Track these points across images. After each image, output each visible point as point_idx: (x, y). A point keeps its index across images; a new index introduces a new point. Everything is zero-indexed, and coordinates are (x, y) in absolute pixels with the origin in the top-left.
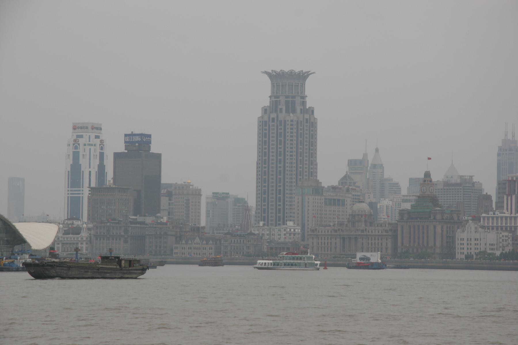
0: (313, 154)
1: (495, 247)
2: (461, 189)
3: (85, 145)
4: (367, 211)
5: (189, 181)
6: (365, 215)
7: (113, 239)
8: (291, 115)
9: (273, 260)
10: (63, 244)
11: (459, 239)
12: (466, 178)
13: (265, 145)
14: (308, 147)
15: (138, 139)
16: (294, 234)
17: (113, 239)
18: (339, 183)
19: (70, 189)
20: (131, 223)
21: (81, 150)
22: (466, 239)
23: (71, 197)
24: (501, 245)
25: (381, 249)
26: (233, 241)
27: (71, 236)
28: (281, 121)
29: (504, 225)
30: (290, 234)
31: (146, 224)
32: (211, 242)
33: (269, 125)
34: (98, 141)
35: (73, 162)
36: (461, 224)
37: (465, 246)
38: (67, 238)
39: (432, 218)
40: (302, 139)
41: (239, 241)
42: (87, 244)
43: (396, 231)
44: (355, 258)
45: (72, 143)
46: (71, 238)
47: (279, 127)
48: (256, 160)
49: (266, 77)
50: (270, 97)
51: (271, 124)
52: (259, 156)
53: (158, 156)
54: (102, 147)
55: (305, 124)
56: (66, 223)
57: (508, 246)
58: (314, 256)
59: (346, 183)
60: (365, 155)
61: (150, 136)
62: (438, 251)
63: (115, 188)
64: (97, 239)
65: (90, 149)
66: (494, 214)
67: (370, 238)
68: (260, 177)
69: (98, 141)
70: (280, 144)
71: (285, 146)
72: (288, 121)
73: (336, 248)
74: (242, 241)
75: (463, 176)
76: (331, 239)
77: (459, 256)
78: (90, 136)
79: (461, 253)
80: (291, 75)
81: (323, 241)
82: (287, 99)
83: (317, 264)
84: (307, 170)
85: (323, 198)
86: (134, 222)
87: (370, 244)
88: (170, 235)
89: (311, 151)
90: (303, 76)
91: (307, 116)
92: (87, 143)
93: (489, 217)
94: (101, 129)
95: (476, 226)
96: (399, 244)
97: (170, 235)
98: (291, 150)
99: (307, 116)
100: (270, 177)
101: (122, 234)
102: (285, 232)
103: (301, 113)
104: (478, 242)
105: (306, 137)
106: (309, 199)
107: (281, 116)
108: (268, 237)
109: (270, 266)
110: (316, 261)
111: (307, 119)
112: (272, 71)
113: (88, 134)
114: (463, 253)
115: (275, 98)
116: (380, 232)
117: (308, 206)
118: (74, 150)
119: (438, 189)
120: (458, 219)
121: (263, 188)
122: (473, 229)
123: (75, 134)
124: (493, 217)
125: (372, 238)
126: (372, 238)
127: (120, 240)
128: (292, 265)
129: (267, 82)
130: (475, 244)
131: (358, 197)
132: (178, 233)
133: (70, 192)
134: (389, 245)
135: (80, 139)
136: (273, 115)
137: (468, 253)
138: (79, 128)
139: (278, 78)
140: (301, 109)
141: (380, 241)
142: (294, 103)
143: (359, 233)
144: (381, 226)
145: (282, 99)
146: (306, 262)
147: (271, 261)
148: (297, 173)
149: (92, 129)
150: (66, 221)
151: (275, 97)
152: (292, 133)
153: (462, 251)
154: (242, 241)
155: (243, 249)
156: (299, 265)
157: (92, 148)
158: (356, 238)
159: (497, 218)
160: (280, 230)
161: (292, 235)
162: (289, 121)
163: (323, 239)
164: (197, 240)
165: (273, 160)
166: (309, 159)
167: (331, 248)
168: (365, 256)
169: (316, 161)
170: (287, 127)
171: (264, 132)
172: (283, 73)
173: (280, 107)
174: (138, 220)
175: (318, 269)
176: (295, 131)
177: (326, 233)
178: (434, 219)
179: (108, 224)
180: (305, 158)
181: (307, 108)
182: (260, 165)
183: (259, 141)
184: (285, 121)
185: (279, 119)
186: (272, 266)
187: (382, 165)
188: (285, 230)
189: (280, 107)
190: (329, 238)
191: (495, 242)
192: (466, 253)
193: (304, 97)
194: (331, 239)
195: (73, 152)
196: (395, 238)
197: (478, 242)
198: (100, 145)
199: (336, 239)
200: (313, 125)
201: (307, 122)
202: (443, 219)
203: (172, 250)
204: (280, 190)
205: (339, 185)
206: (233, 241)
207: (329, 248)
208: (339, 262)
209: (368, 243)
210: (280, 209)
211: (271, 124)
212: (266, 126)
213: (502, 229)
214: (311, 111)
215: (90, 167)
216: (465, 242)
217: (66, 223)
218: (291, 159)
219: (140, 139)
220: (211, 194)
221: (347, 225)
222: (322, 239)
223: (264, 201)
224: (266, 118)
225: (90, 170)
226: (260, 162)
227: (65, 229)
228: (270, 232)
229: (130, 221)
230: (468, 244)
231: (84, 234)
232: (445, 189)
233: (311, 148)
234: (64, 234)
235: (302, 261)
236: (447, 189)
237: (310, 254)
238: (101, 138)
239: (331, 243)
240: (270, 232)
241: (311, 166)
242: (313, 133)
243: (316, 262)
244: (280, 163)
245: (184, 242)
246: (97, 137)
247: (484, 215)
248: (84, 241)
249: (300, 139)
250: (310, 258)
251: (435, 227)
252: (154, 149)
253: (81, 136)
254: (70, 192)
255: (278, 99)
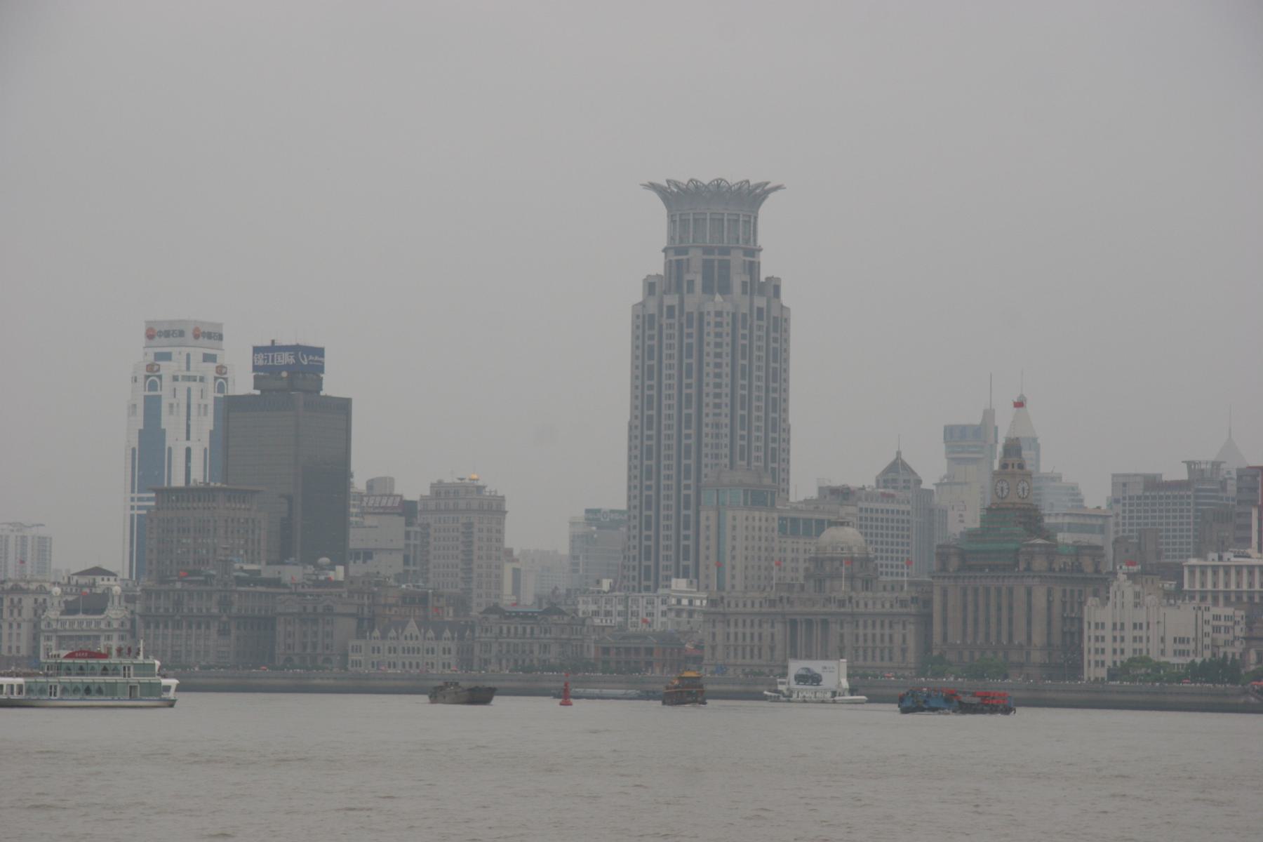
0: (777, 403)
1: (1192, 646)
2: (1189, 497)
3: (175, 379)
4: (855, 549)
5: (475, 476)
6: (851, 560)
7: (190, 627)
8: (718, 298)
9: (24, 675)
10: (61, 638)
11: (1093, 626)
12: (1203, 466)
13: (651, 378)
14: (763, 384)
15: (287, 359)
16: (691, 614)
17: (190, 627)
18: (878, 481)
19: (136, 495)
20: (240, 581)
21: (165, 392)
22: (1109, 625)
23: (139, 515)
24: (1207, 641)
25: (891, 652)
26: (505, 631)
27: (81, 616)
28: (690, 315)
29: (1233, 587)
30: (679, 613)
31: (285, 586)
32: (447, 634)
33: (661, 326)
34: (210, 370)
35: (145, 425)
36: (1100, 583)
37: (1108, 645)
38: (72, 623)
39: (1021, 568)
40: (746, 362)
41: (520, 630)
42: (122, 638)
43: (928, 603)
44: (784, 675)
45: (142, 372)
46: (81, 623)
47: (685, 330)
48: (628, 417)
49: (654, 197)
50: (665, 250)
51: (665, 321)
52: (634, 407)
53: (343, 407)
54: (221, 384)
55: (756, 323)
56: (73, 582)
57: (1233, 642)
58: (157, 663)
59: (894, 481)
60: (989, 414)
61: (320, 352)
62: (1037, 656)
63: (219, 489)
64: (148, 626)
65: (189, 390)
66: (1220, 558)
67: (861, 623)
68: (637, 462)
69: (210, 370)
70: (689, 376)
71: (700, 380)
72: (709, 313)
73: (772, 649)
74: (528, 631)
75: (1194, 463)
76: (760, 625)
77: (1092, 672)
78: (188, 355)
79: (1097, 662)
80: (718, 192)
81: (740, 630)
82: (705, 257)
83: (167, 688)
84: (761, 444)
85: (776, 515)
86: (254, 579)
87: (861, 638)
88: (344, 615)
89: (772, 395)
90: (751, 197)
91: (760, 302)
92: (180, 374)
93: (1206, 566)
94: (220, 337)
95: (1138, 588)
96: (937, 639)
97: (344, 615)
98: (717, 391)
99: (760, 302)
100: (664, 462)
101: (215, 611)
102: (664, 608)
103: (744, 292)
104: (1143, 633)
105: (759, 358)
106: (734, 519)
107: (691, 302)
108: (620, 619)
109: (15, 696)
110: (165, 677)
111: (760, 310)
112: (668, 181)
113: (185, 350)
114: (1103, 663)
115: (676, 251)
116: (887, 605)
117: (734, 538)
118: (147, 393)
119: (1131, 498)
120: (1097, 571)
121: (645, 493)
122: (1129, 597)
123: (151, 351)
124: (1218, 566)
125: (865, 622)
126: (865, 622)
127: (208, 627)
128: (88, 691)
129: (657, 212)
130: (1135, 639)
131: (905, 517)
132: (366, 610)
133: (136, 504)
134: (911, 643)
135: (163, 364)
136: (672, 300)
137: (1115, 663)
138: (161, 334)
139: (678, 198)
140: (744, 284)
141: (887, 631)
142: (725, 266)
143: (833, 608)
144: (893, 589)
145: (696, 257)
146: (134, 680)
147: (20, 680)
148: (732, 453)
149: (196, 336)
150: (75, 578)
151: (679, 251)
152: (718, 345)
153: (1100, 658)
154: (528, 631)
155: (532, 652)
156: (112, 690)
157: (195, 386)
158: (825, 623)
159: (1227, 569)
160: (651, 602)
161: (685, 615)
162: (712, 314)
163: (740, 624)
164: (412, 628)
165: (669, 417)
166: (766, 414)
167: (760, 650)
168: (808, 669)
169: (785, 420)
170: (706, 329)
171: (648, 343)
172: (697, 187)
173: (687, 277)
174: (264, 575)
175: (171, 704)
176: (729, 339)
177: (749, 609)
178: (1028, 569)
179: (178, 585)
180: (755, 414)
181: (762, 279)
182: (638, 432)
183: (635, 367)
184: (701, 315)
185: (687, 309)
186: (23, 696)
187: (1035, 440)
188: (664, 602)
189: (687, 277)
190: (756, 622)
191: (1192, 635)
192: (1109, 663)
193: (753, 252)
194: (760, 625)
195: (146, 397)
196: (925, 620)
197: (1143, 633)
198: (216, 379)
199: (773, 626)
200: (778, 324)
201: (760, 317)
202: (1051, 569)
203: (345, 655)
204: (687, 497)
205: (878, 487)
206: (505, 631)
207: (756, 651)
208: (589, 691)
209: (728, 634)
210: (687, 548)
211: (665, 321)
212: (651, 328)
213: (1227, 598)
214: (774, 288)
215: (188, 438)
216: (1108, 633)
217: (73, 582)
218: (715, 415)
219: (292, 361)
220: (583, 513)
221: (802, 587)
222: (736, 625)
223: (648, 527)
224: (652, 308)
225: (188, 444)
226: (638, 422)
227: (70, 598)
228: (627, 607)
229: (237, 577)
230: (1115, 639)
231: (115, 613)
232: (1147, 498)
233: (772, 385)
234: (62, 613)
235: (119, 679)
236: (1154, 498)
237: (146, 657)
238: (219, 361)
239: (760, 635)
240: (627, 607)
241: (771, 435)
242: (777, 345)
243: (165, 682)
244: (688, 427)
245: (377, 633)
246: (208, 358)
247: (1193, 561)
248: (115, 630)
249: (741, 362)
250: (146, 669)
251: (1029, 593)
252: (332, 386)
253: (167, 357)
254: (136, 504)
255: (684, 257)
